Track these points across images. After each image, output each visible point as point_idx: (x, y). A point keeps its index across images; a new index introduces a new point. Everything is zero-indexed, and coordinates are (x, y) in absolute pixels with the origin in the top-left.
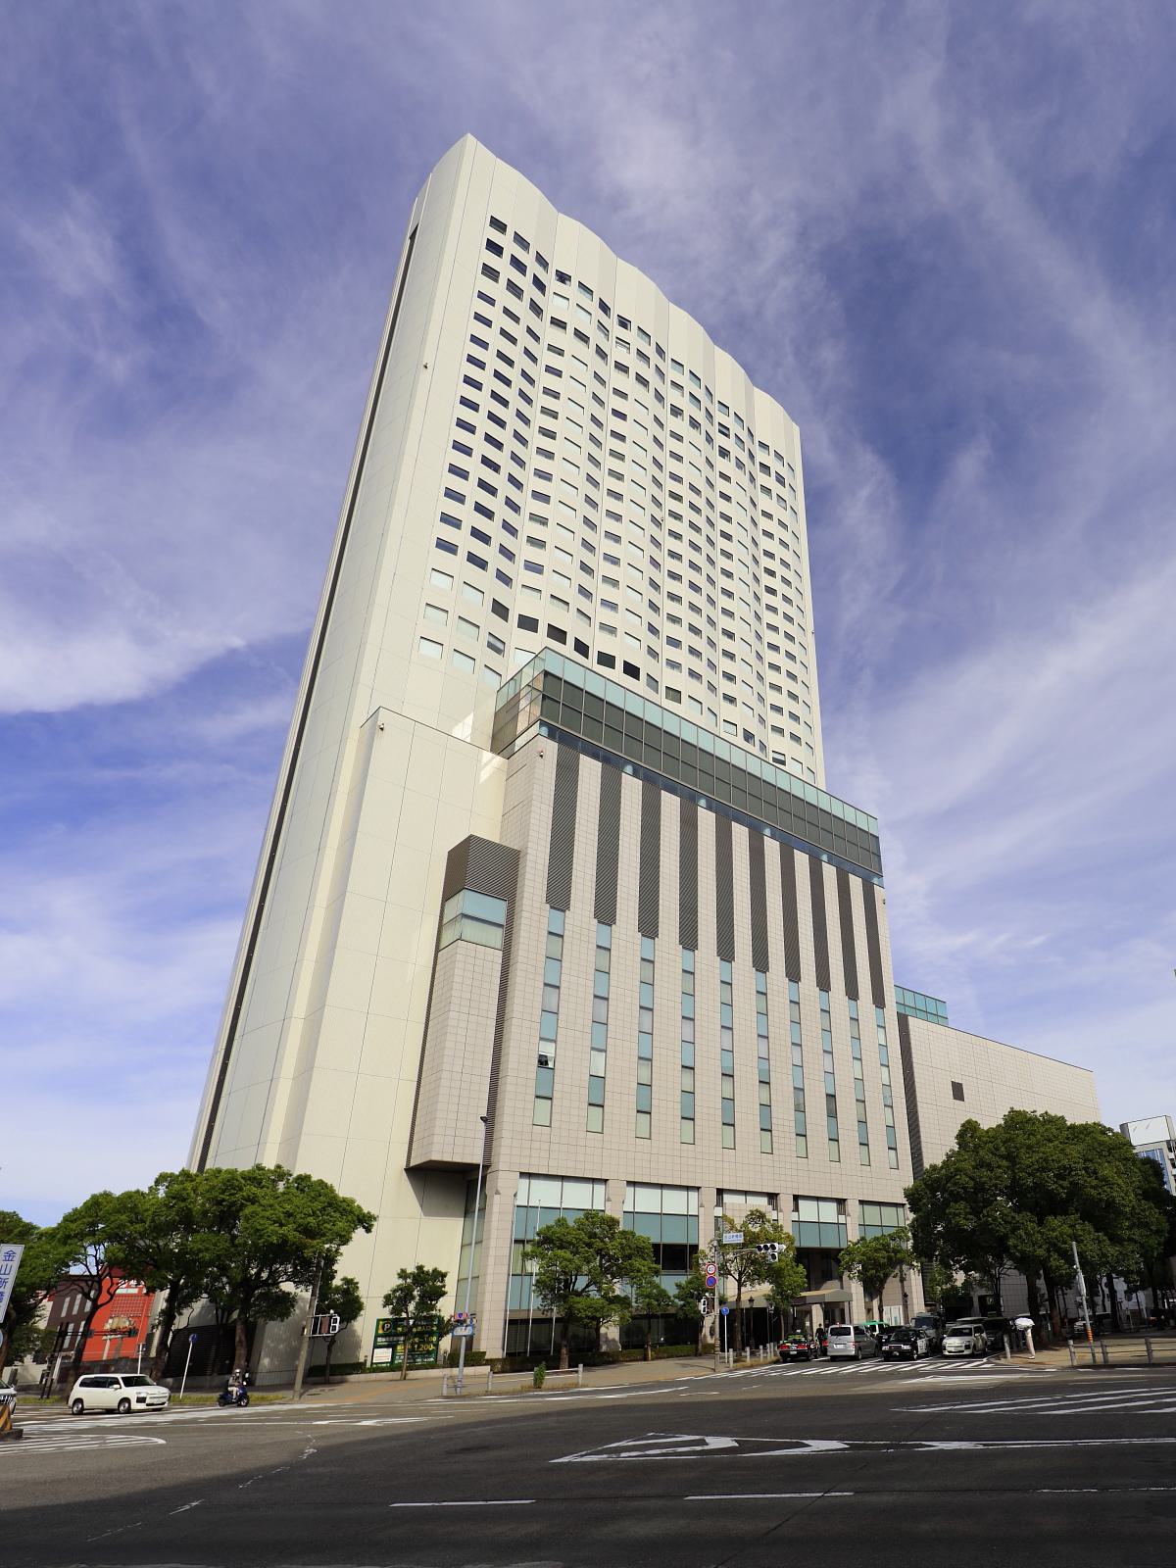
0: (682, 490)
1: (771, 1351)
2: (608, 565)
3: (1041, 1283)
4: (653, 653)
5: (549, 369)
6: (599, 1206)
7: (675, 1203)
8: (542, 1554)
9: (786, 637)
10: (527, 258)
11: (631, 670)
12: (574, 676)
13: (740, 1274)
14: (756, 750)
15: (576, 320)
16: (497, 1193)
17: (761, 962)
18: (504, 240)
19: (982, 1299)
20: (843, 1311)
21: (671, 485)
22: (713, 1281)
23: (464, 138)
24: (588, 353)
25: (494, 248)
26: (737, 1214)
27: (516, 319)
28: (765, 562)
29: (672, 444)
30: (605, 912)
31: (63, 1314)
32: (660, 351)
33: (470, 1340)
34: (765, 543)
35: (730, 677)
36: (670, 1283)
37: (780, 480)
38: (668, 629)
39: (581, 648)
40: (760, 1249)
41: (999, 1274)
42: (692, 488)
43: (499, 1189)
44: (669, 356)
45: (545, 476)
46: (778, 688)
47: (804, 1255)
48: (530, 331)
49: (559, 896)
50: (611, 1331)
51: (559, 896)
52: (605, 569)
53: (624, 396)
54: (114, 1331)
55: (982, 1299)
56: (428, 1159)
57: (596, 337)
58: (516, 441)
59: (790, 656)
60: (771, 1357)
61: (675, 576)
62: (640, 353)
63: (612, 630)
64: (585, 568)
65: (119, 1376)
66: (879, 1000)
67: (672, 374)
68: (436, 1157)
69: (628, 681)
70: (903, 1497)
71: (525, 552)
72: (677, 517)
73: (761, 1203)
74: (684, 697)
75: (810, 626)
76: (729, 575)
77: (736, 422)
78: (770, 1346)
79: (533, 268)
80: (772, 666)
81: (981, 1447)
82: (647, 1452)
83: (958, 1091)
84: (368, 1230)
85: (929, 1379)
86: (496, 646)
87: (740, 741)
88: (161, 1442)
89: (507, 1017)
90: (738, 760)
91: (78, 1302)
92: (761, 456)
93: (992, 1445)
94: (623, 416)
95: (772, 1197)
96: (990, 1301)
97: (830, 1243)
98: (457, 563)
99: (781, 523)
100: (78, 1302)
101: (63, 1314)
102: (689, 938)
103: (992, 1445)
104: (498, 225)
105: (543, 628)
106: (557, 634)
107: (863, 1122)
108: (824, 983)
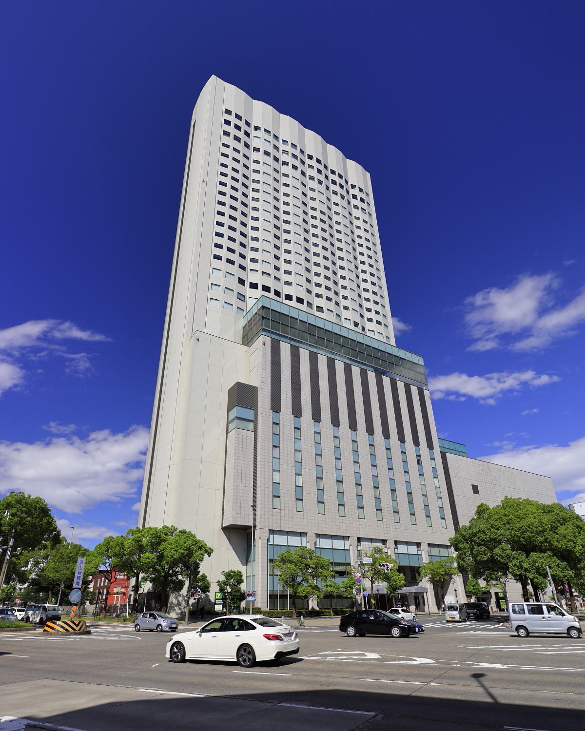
0: (316, 214)
3: (530, 588)
4: (309, 291)
6: (304, 545)
7: (338, 544)
8: (569, 689)
10: (241, 124)
11: (300, 301)
12: (275, 306)
13: (372, 578)
15: (263, 146)
17: (370, 431)
18: (232, 118)
19: (497, 594)
20: (423, 597)
22: (359, 580)
24: (270, 160)
26: (368, 549)
27: (239, 152)
30: (317, 417)
31: (98, 586)
33: (253, 602)
36: (340, 582)
40: (380, 565)
41: (505, 581)
42: (321, 212)
47: (401, 569)
48: (245, 156)
49: (276, 407)
50: (313, 604)
51: (276, 407)
54: (117, 593)
55: (497, 594)
65: (16, 608)
66: (430, 446)
69: (299, 306)
70: (468, 689)
73: (380, 545)
74: (325, 310)
79: (244, 127)
81: (506, 667)
82: (339, 657)
83: (475, 489)
84: (209, 556)
85: (472, 632)
86: (241, 297)
87: (352, 327)
88: (140, 639)
90: (352, 336)
91: (103, 581)
93: (513, 667)
95: (384, 542)
96: (501, 595)
97: (414, 564)
100: (103, 581)
101: (98, 586)
102: (317, 417)
103: (513, 667)
104: (228, 112)
105: (260, 287)
106: (266, 289)
107: (426, 506)
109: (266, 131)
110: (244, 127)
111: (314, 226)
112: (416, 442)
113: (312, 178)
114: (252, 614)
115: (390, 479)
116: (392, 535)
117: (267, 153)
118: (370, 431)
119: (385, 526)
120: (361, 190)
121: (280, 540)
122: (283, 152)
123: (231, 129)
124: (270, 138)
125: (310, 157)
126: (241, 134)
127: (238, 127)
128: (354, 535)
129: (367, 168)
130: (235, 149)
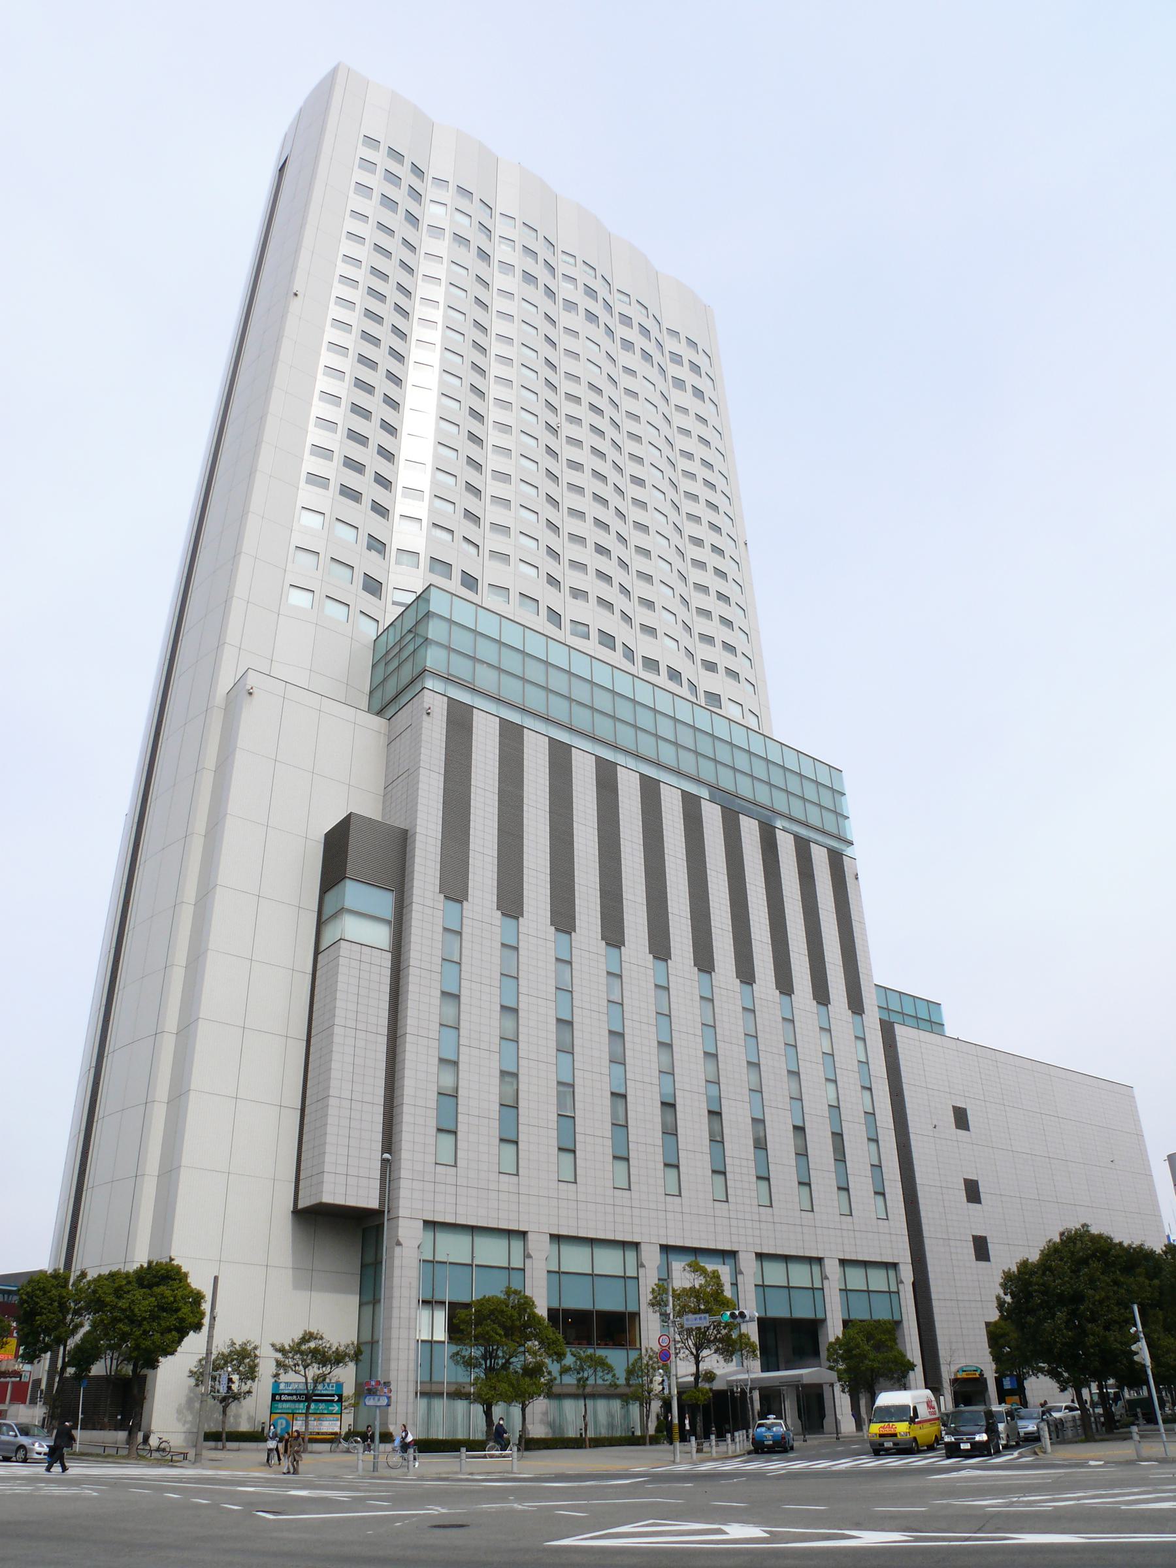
1: (740, 1440)
9: (716, 573)
10: (404, 171)
11: (674, 675)
14: (684, 691)
16: (399, 1244)
23: (340, 885)
35: (649, 604)
43: (400, 1239)
44: (560, 247)
56: (318, 1201)
60: (739, 1448)
63: (504, 557)
66: (856, 1004)
68: (327, 1199)
69: (604, 653)
78: (740, 1435)
83: (973, 1192)
89: (400, 1032)
92: (671, 345)
104: (371, 142)
108: (785, 984)
110: (408, 178)
111: (574, 420)
113: (570, 305)
115: (829, 1105)
116: (750, 1240)
121: (454, 1248)
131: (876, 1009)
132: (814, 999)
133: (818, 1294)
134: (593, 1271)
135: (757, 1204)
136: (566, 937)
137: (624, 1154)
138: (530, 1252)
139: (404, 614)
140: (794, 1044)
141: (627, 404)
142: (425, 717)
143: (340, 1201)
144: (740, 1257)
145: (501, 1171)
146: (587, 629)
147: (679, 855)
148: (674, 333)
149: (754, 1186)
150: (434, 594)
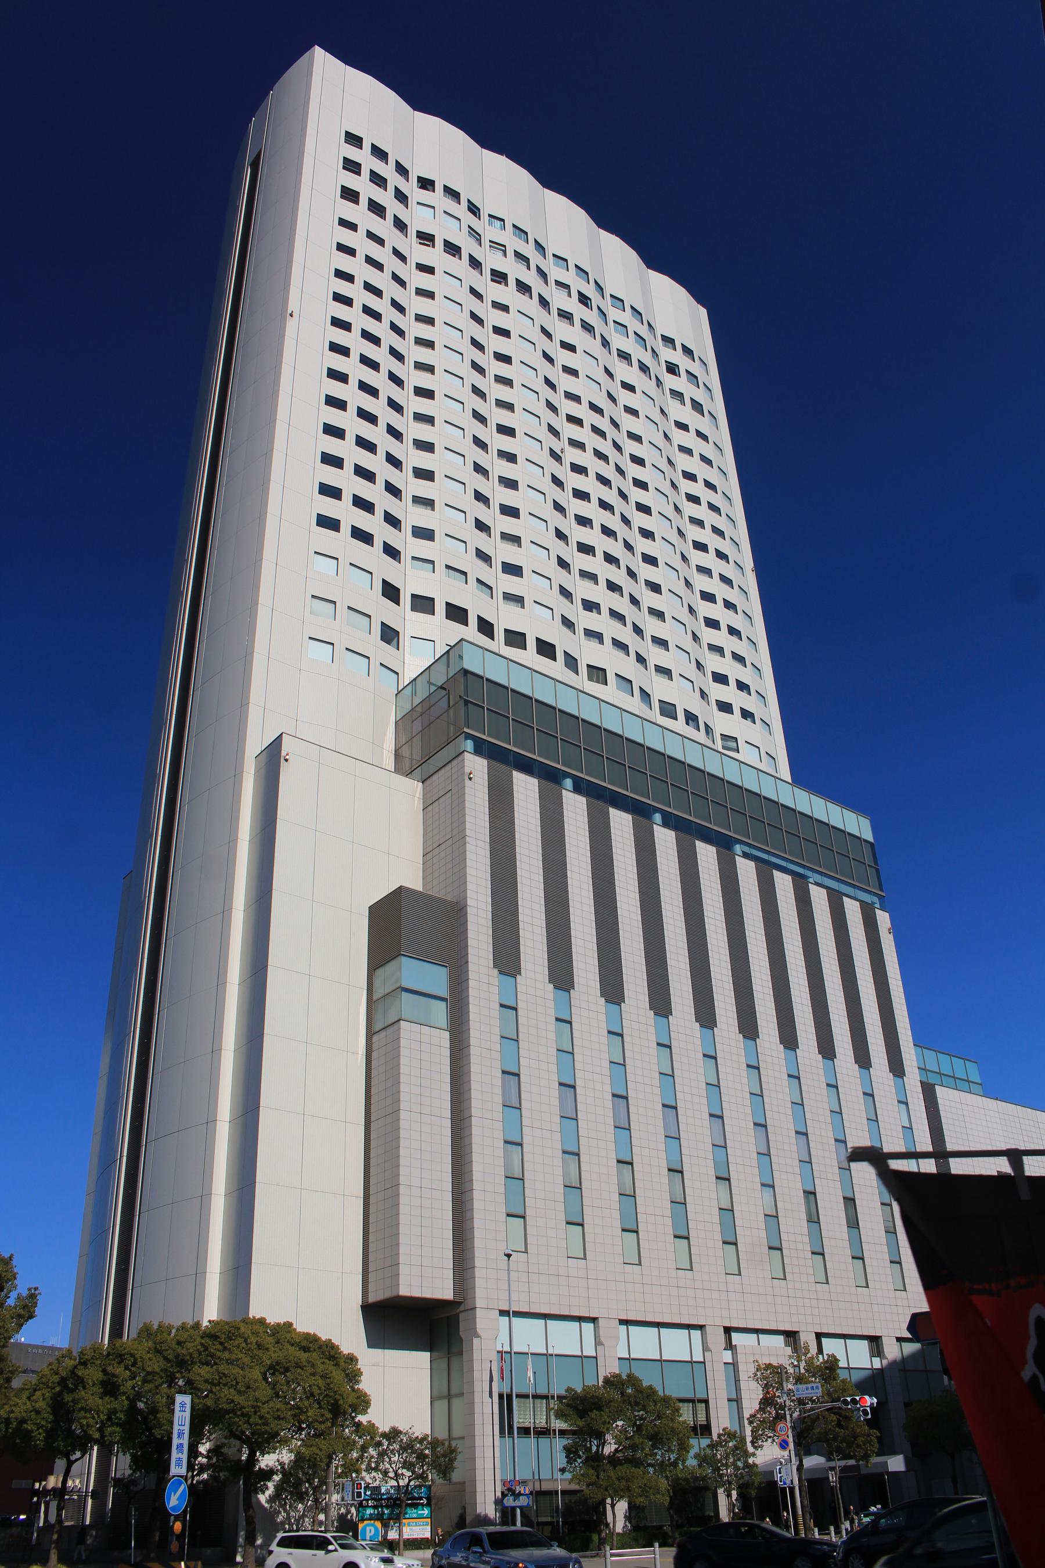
0: (580, 411)
2: (504, 463)
4: (567, 623)
5: (420, 292)
10: (387, 171)
11: (546, 649)
15: (444, 230)
18: (363, 156)
21: (568, 407)
23: (313, 48)
25: (352, 166)
27: (381, 242)
28: (686, 486)
29: (563, 357)
32: (540, 247)
34: (684, 462)
37: (697, 406)
38: (579, 534)
39: (486, 627)
42: (593, 407)
45: (426, 447)
46: (719, 650)
48: (396, 252)
52: (503, 496)
53: (505, 308)
56: (394, 1294)
57: (468, 246)
58: (396, 200)
59: (721, 555)
61: (581, 495)
62: (517, 254)
64: (481, 526)
66: (897, 1068)
67: (555, 273)
68: (404, 1291)
69: (542, 663)
71: (413, 516)
72: (580, 445)
75: (748, 562)
76: (636, 438)
77: (636, 342)
79: (394, 180)
80: (701, 569)
92: (667, 354)
94: (506, 333)
98: (341, 542)
99: (699, 434)
104: (354, 140)
106: (457, 614)
108: (706, 1016)
109: (450, 192)
112: (863, 1059)
114: (63, 1348)
117: (452, 249)
118: (748, 1027)
119: (791, 1293)
120: (687, 351)
122: (490, 246)
123: (361, 184)
124: (461, 210)
125: (426, 184)
126: (385, 198)
127: (378, 180)
128: (715, 1320)
129: (699, 297)
130: (371, 235)
131: (917, 1071)
132: (856, 1062)
133: (589, 1364)
134: (692, 1359)
135: (675, 1268)
136: (616, 1007)
137: (684, 1233)
138: (602, 1339)
139: (431, 668)
140: (622, 1062)
141: (628, 423)
142: (467, 781)
143: (416, 1293)
144: (884, 1342)
145: (773, 1277)
146: (674, 708)
147: (718, 917)
148: (668, 341)
149: (809, 1263)
150: (467, 649)
